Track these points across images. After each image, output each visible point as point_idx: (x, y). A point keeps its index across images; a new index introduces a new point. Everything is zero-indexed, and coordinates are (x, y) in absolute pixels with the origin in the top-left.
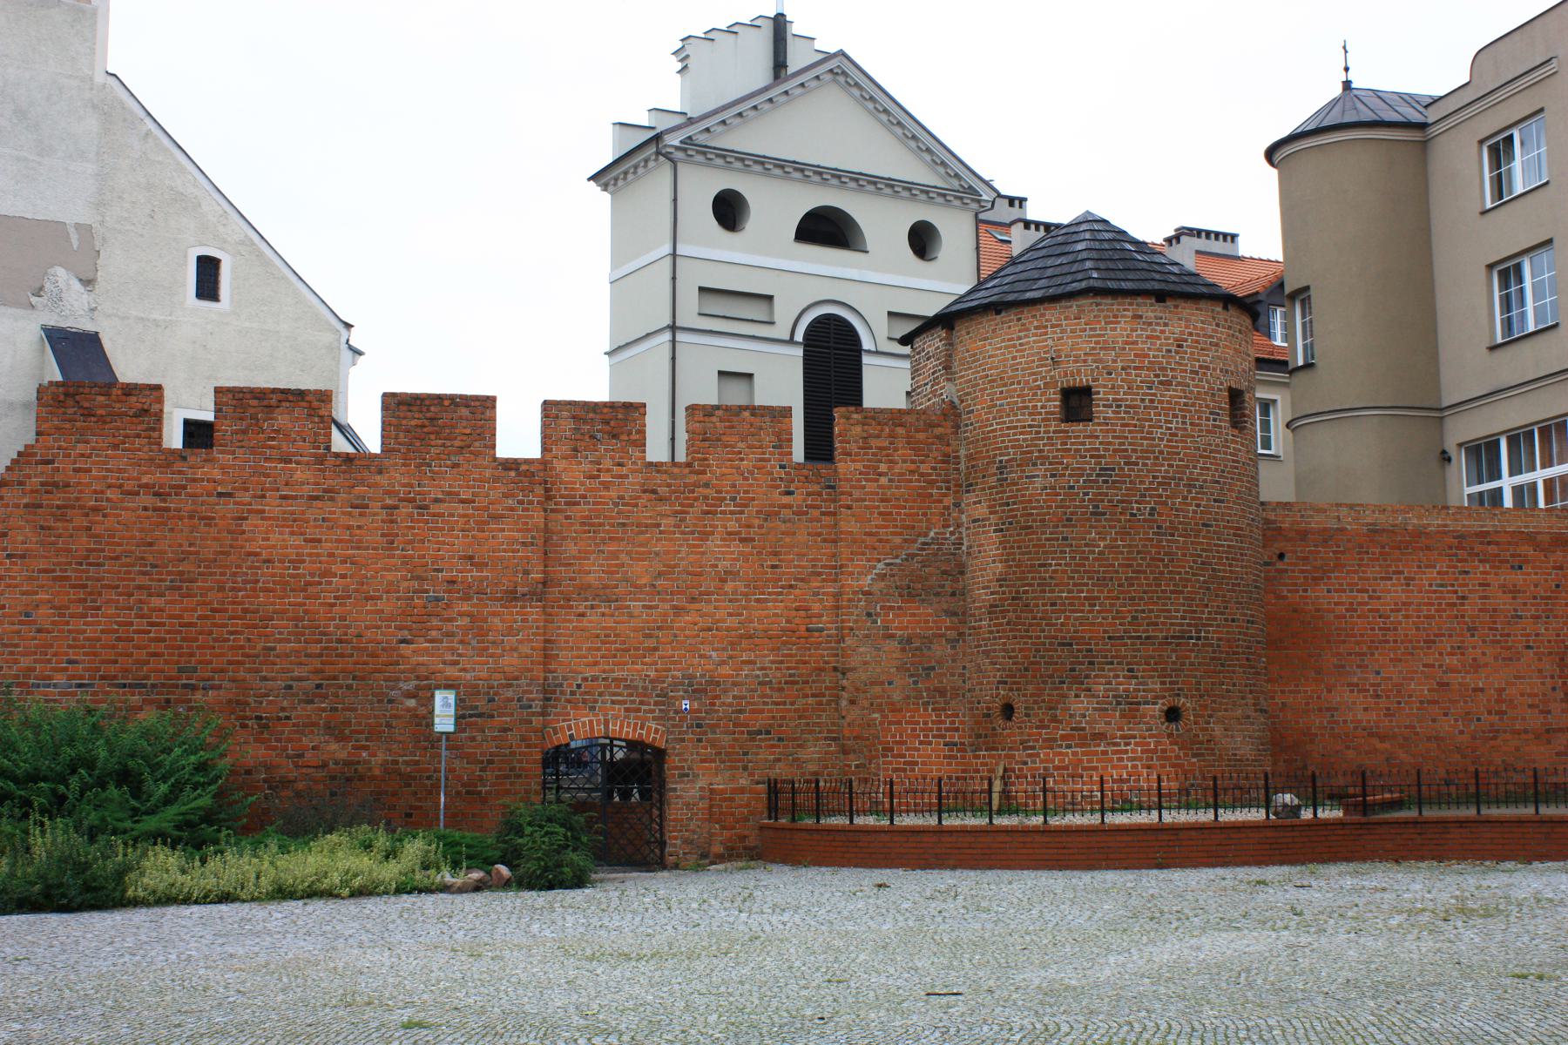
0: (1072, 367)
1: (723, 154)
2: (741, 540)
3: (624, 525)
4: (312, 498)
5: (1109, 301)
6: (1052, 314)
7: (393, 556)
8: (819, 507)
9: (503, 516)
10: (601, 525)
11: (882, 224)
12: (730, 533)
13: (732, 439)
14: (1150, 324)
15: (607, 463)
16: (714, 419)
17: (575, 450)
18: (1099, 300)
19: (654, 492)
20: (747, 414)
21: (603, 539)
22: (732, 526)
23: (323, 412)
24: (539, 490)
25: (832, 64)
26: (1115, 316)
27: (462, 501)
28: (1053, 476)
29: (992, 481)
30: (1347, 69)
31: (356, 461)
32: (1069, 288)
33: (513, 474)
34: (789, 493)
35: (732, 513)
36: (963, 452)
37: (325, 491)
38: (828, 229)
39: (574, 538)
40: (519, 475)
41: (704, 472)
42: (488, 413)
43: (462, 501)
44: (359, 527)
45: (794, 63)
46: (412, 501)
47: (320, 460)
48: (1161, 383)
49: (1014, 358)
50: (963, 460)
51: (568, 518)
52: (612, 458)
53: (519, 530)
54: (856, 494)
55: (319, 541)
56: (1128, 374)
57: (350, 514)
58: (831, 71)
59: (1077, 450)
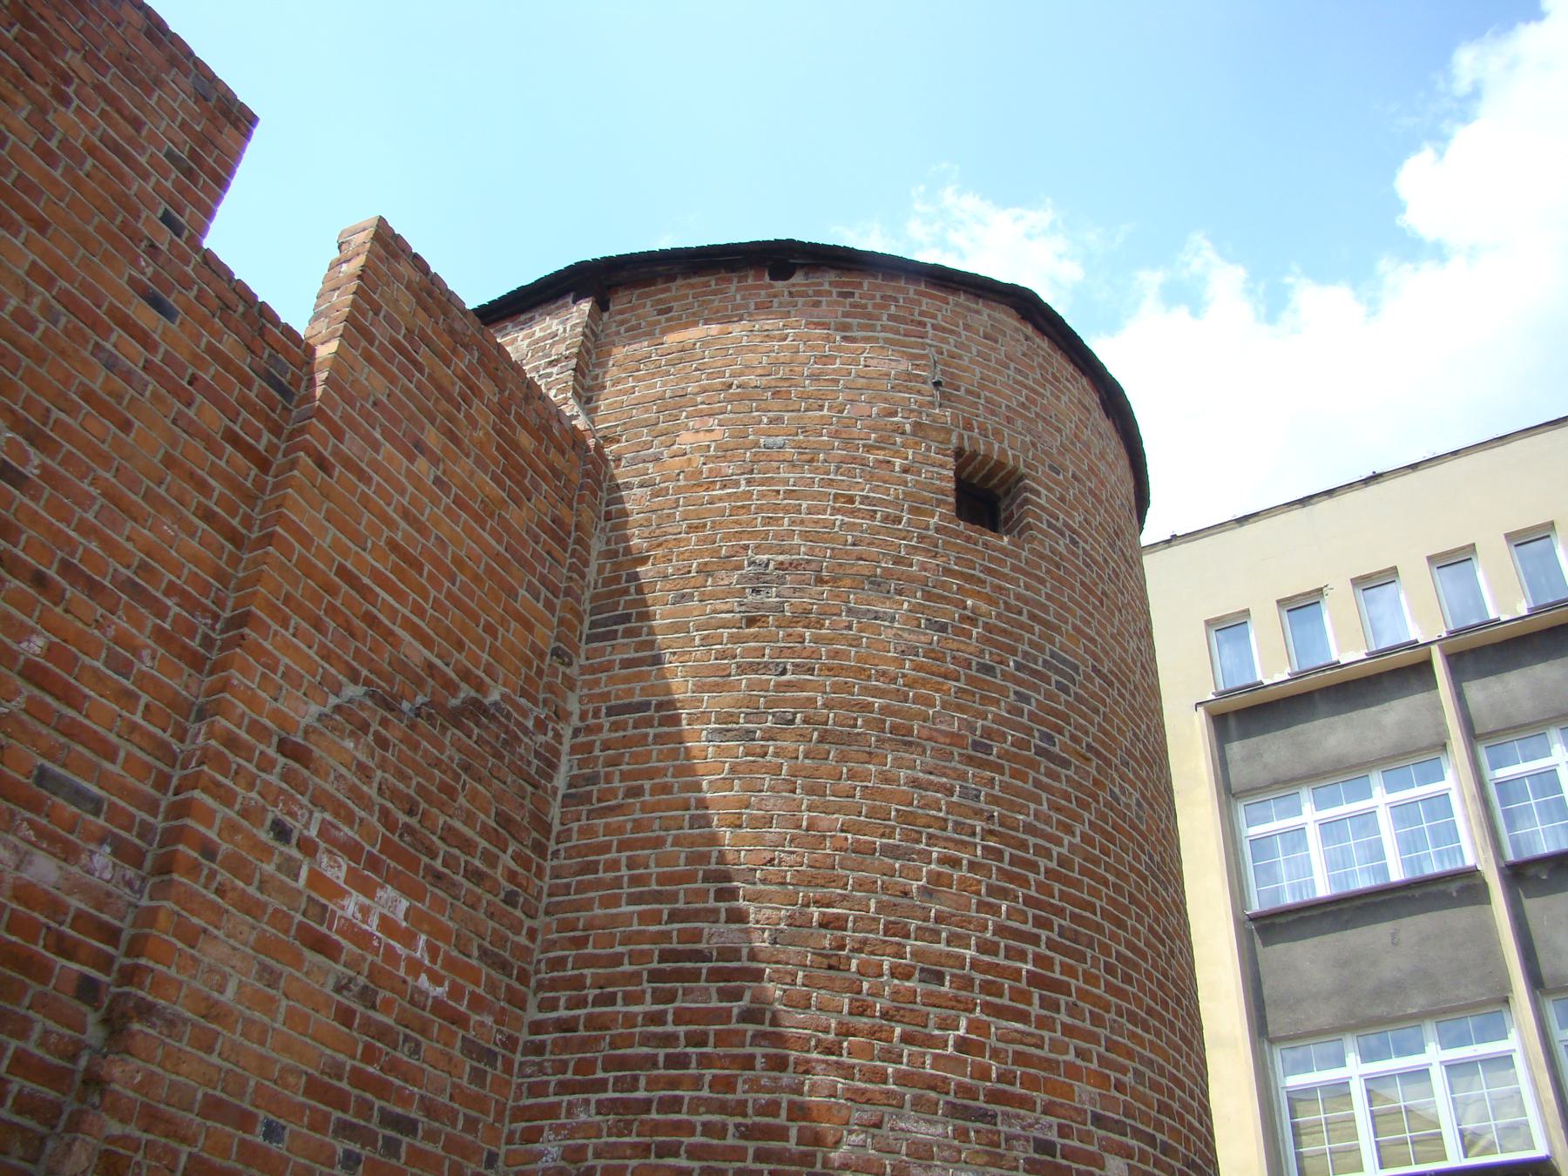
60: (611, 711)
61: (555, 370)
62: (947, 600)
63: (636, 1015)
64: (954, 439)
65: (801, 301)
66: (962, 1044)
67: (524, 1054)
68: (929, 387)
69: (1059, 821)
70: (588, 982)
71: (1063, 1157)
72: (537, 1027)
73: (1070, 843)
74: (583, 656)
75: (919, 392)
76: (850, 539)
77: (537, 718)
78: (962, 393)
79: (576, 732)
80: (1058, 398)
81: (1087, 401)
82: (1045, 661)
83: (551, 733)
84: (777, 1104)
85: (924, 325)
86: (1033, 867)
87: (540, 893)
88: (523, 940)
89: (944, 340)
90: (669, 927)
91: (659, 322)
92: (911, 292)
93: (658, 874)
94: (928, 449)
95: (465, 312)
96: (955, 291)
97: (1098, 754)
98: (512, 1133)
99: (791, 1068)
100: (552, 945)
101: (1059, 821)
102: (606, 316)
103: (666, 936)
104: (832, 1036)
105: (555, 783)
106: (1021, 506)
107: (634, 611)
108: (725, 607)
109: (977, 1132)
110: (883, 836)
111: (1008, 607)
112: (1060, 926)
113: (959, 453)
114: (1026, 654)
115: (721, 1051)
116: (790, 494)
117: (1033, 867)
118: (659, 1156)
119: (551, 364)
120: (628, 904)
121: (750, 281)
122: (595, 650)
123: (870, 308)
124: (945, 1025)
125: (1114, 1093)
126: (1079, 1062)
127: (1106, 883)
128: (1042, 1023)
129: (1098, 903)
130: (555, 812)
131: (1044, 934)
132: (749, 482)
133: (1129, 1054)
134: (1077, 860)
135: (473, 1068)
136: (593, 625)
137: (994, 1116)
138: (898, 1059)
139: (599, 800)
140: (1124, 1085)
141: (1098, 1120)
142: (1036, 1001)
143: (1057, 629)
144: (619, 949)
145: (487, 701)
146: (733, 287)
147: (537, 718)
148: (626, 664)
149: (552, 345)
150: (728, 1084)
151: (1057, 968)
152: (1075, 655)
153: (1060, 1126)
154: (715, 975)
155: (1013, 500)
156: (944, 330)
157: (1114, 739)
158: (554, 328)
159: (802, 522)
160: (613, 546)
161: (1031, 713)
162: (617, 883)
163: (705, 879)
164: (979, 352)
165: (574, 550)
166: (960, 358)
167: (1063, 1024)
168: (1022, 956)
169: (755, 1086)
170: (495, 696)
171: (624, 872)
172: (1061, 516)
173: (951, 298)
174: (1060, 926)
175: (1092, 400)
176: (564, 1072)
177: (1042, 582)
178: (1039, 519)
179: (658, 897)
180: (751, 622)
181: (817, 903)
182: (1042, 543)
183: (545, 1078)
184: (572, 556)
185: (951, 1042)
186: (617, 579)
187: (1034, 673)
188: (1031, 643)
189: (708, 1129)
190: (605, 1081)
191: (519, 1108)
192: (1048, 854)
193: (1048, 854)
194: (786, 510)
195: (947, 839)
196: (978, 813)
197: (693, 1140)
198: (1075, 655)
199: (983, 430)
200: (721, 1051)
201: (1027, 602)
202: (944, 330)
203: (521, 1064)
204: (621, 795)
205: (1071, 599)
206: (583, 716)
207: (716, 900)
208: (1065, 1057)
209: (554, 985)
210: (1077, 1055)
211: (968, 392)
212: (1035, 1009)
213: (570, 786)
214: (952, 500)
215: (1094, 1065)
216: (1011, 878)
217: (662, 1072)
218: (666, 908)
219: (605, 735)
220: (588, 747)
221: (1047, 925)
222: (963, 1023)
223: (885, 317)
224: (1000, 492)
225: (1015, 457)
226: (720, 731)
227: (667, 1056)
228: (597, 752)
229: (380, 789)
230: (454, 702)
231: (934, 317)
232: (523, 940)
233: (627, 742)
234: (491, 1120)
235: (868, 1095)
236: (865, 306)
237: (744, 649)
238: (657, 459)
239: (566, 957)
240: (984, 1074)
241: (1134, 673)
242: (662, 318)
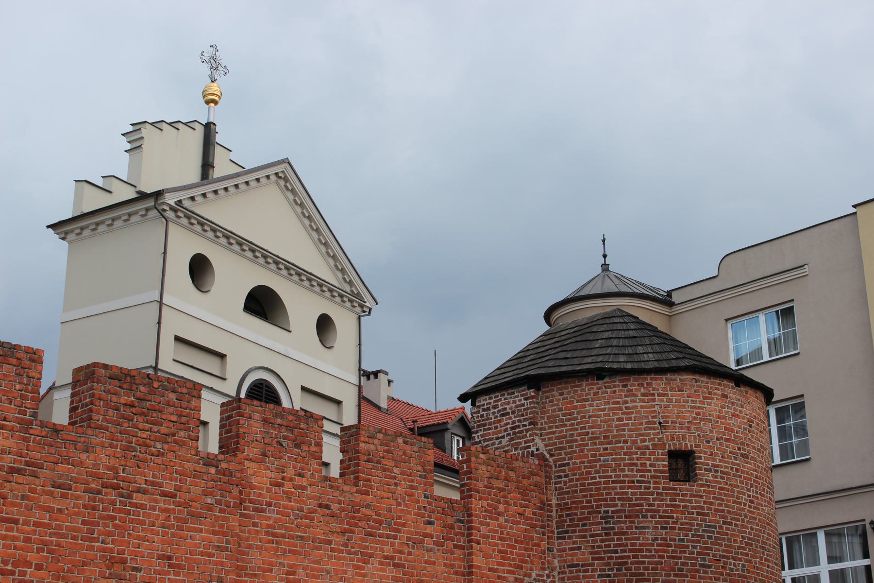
0: (678, 432)
1: (203, 222)
2: (396, 565)
3: (302, 538)
4: (12, 470)
5: (705, 379)
6: (659, 384)
7: (91, 548)
8: (452, 539)
9: (200, 515)
10: (283, 536)
11: (302, 306)
12: (386, 557)
13: (390, 463)
14: (733, 404)
15: (290, 472)
16: (376, 442)
17: (264, 455)
18: (697, 377)
19: (327, 507)
20: (400, 440)
21: (284, 551)
22: (388, 550)
23: (32, 373)
24: (235, 492)
25: (278, 169)
26: (710, 393)
27: (164, 494)
28: (663, 528)
29: (597, 529)
30: (605, 256)
31: (56, 430)
32: (674, 363)
33: (213, 470)
34: (430, 523)
35: (388, 537)
36: (554, 502)
37: (27, 464)
38: (262, 304)
39: (259, 548)
40: (218, 472)
41: (367, 493)
42: (193, 403)
43: (164, 494)
44: (60, 511)
45: (218, 171)
46: (116, 487)
47: (26, 425)
48: (742, 455)
49: (620, 420)
50: (554, 509)
51: (255, 525)
52: (295, 467)
53: (215, 533)
54: (484, 530)
55: (16, 522)
56: (721, 444)
57: (51, 494)
58: (277, 174)
59: (685, 507)
60: (569, 566)
68: (657, 425)
79: (559, 573)
121: (590, 382)
148: (571, 549)
225: (691, 446)
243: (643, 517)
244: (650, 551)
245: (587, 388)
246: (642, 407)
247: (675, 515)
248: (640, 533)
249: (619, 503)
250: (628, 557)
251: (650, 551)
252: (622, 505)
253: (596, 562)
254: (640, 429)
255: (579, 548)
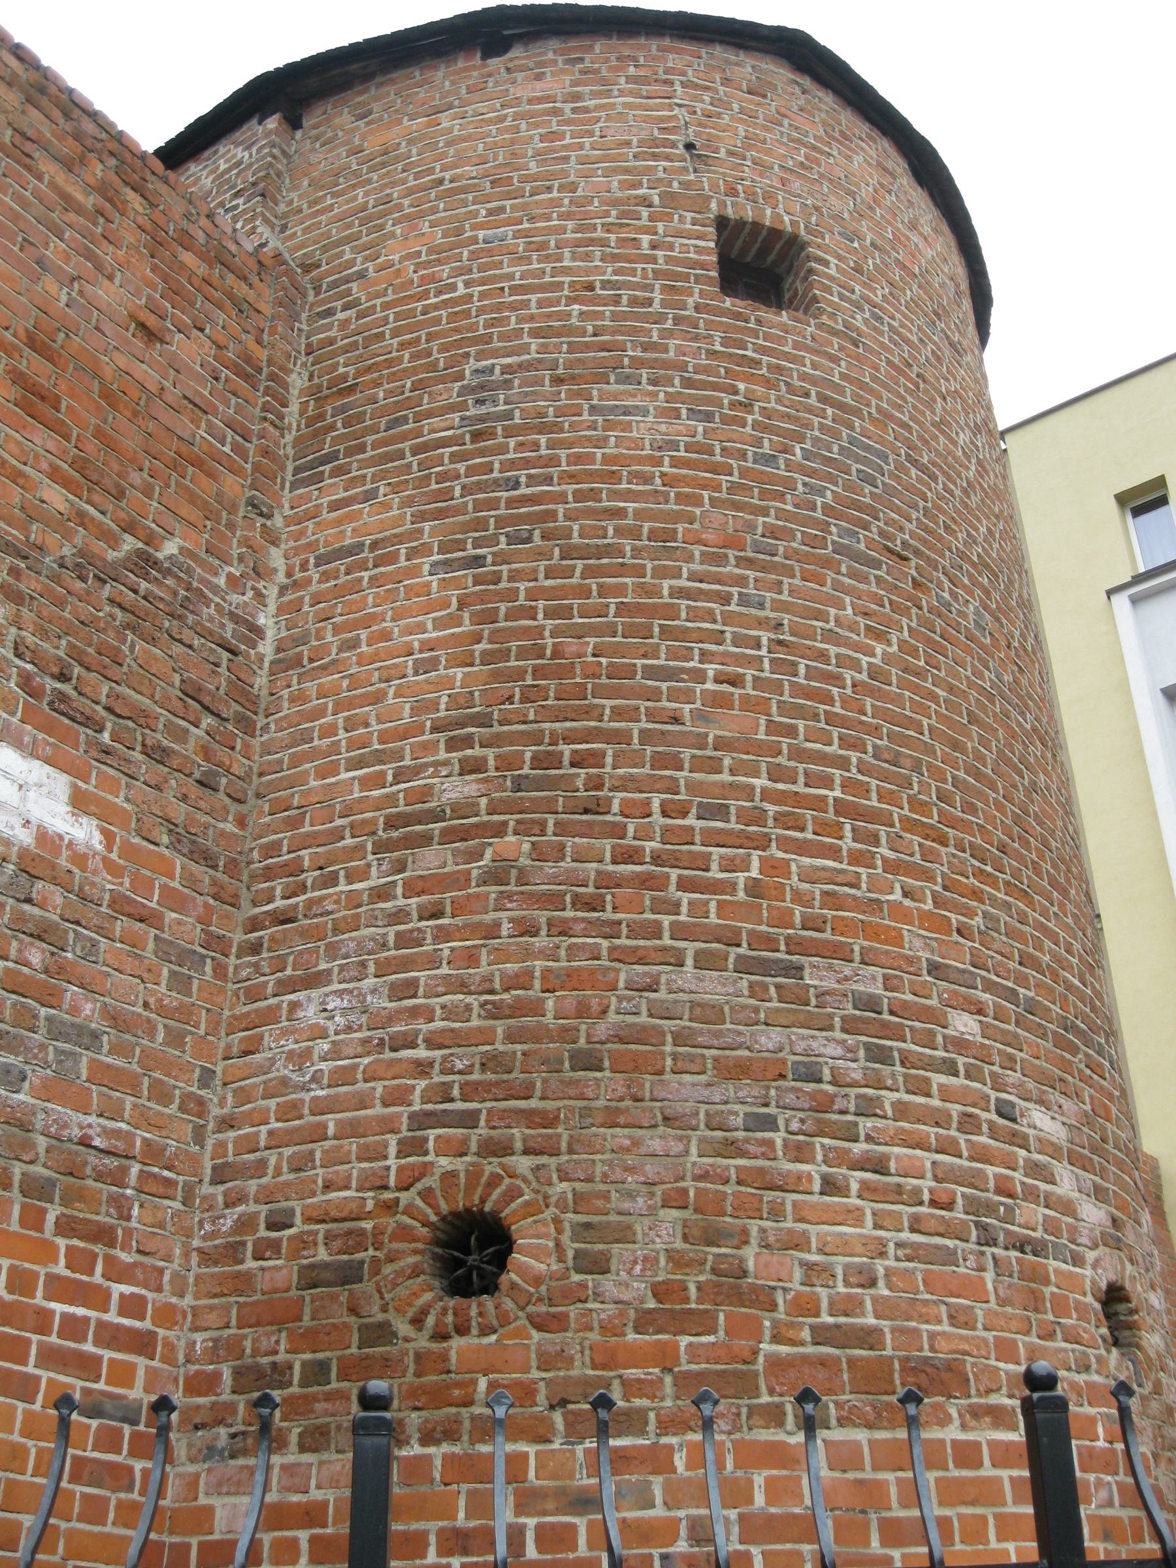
61: (241, 201)
62: (715, 387)
63: (359, 892)
64: (714, 205)
65: (520, 76)
66: (754, 888)
67: (238, 957)
68: (680, 150)
69: (868, 628)
70: (306, 863)
71: (892, 1013)
72: (254, 925)
73: (884, 653)
74: (287, 506)
75: (668, 158)
76: (590, 329)
77: (230, 576)
78: (722, 154)
79: (283, 590)
80: (848, 158)
81: (890, 165)
82: (841, 448)
83: (250, 594)
84: (529, 973)
85: (671, 83)
86: (837, 680)
87: (249, 774)
88: (229, 827)
89: (694, 98)
90: (395, 788)
91: (358, 128)
92: (654, 48)
93: (380, 731)
94: (682, 219)
95: (143, 156)
96: (710, 41)
97: (917, 552)
98: (229, 1046)
99: (544, 932)
100: (268, 829)
101: (868, 628)
102: (299, 134)
103: (391, 799)
104: (591, 890)
105: (261, 648)
106: (806, 279)
107: (341, 447)
108: (443, 425)
109: (778, 987)
110: (645, 656)
111: (790, 389)
112: (875, 746)
113: (722, 223)
114: (816, 440)
115: (459, 921)
116: (514, 290)
117: (837, 680)
118: (394, 1049)
119: (237, 195)
120: (348, 770)
122: (301, 496)
123: (604, 73)
124: (729, 866)
125: (955, 937)
126: (907, 902)
127: (934, 698)
128: (856, 858)
129: (925, 722)
130: (261, 681)
131: (854, 756)
132: (467, 284)
133: (976, 895)
134: (894, 671)
135: (173, 974)
136: (297, 470)
137: (801, 968)
138: (675, 908)
139: (311, 660)
140: (969, 928)
141: (934, 969)
142: (848, 833)
143: (857, 412)
144: (339, 822)
145: (160, 556)
146: (440, 74)
147: (230, 576)
148: (334, 506)
149: (238, 175)
150: (471, 958)
151: (874, 795)
152: (882, 441)
153: (886, 978)
154: (449, 836)
155: (796, 275)
156: (696, 86)
157: (940, 539)
158: (239, 156)
159: (532, 318)
160: (316, 381)
161: (825, 506)
162: (335, 748)
163: (435, 729)
164: (741, 108)
165: (267, 387)
166: (719, 116)
167: (883, 859)
168: (828, 783)
169: (500, 955)
170: (170, 548)
171: (342, 734)
172: (857, 288)
173: (703, 52)
174: (875, 746)
175: (898, 164)
176: (282, 970)
177: (835, 360)
178: (828, 289)
179: (380, 758)
180: (476, 436)
181: (567, 740)
182: (832, 316)
183: (263, 979)
184: (266, 394)
185: (741, 886)
186: (321, 417)
187: (829, 461)
188: (822, 427)
189: (450, 1013)
190: (329, 972)
191: (235, 1017)
192: (856, 666)
193: (856, 666)
194: (513, 307)
195: (726, 654)
196: (761, 623)
197: (432, 1026)
198: (882, 441)
199: (751, 196)
200: (459, 921)
201: (814, 381)
202: (696, 86)
203: (236, 967)
204: (334, 650)
205: (874, 379)
206: (289, 575)
207: (448, 751)
208: (891, 897)
209: (269, 874)
210: (906, 894)
211: (731, 153)
212: (848, 843)
213: (279, 650)
214: (714, 274)
215: (929, 906)
216: (809, 694)
217: (393, 952)
218: (389, 769)
219: (314, 588)
220: (296, 606)
221: (860, 747)
222: (755, 863)
223: (622, 80)
224: (780, 270)
226: (446, 563)
227: (398, 934)
228: (306, 608)
229: (16, 649)
230: (111, 555)
231: (684, 74)
232: (229, 827)
233: (339, 592)
234: (202, 1032)
235: (640, 953)
236: (598, 71)
237: (468, 467)
238: (361, 275)
239: (280, 841)
240: (784, 919)
241: (968, 469)
242: (361, 123)
243: (626, 379)
244: (647, 479)
245: (444, 79)
246: (625, 105)
247: (741, 386)
248: (609, 426)
249: (535, 343)
250: (561, 498)
251: (647, 479)
252: (543, 349)
253: (427, 526)
254: (623, 158)
255: (369, 496)
